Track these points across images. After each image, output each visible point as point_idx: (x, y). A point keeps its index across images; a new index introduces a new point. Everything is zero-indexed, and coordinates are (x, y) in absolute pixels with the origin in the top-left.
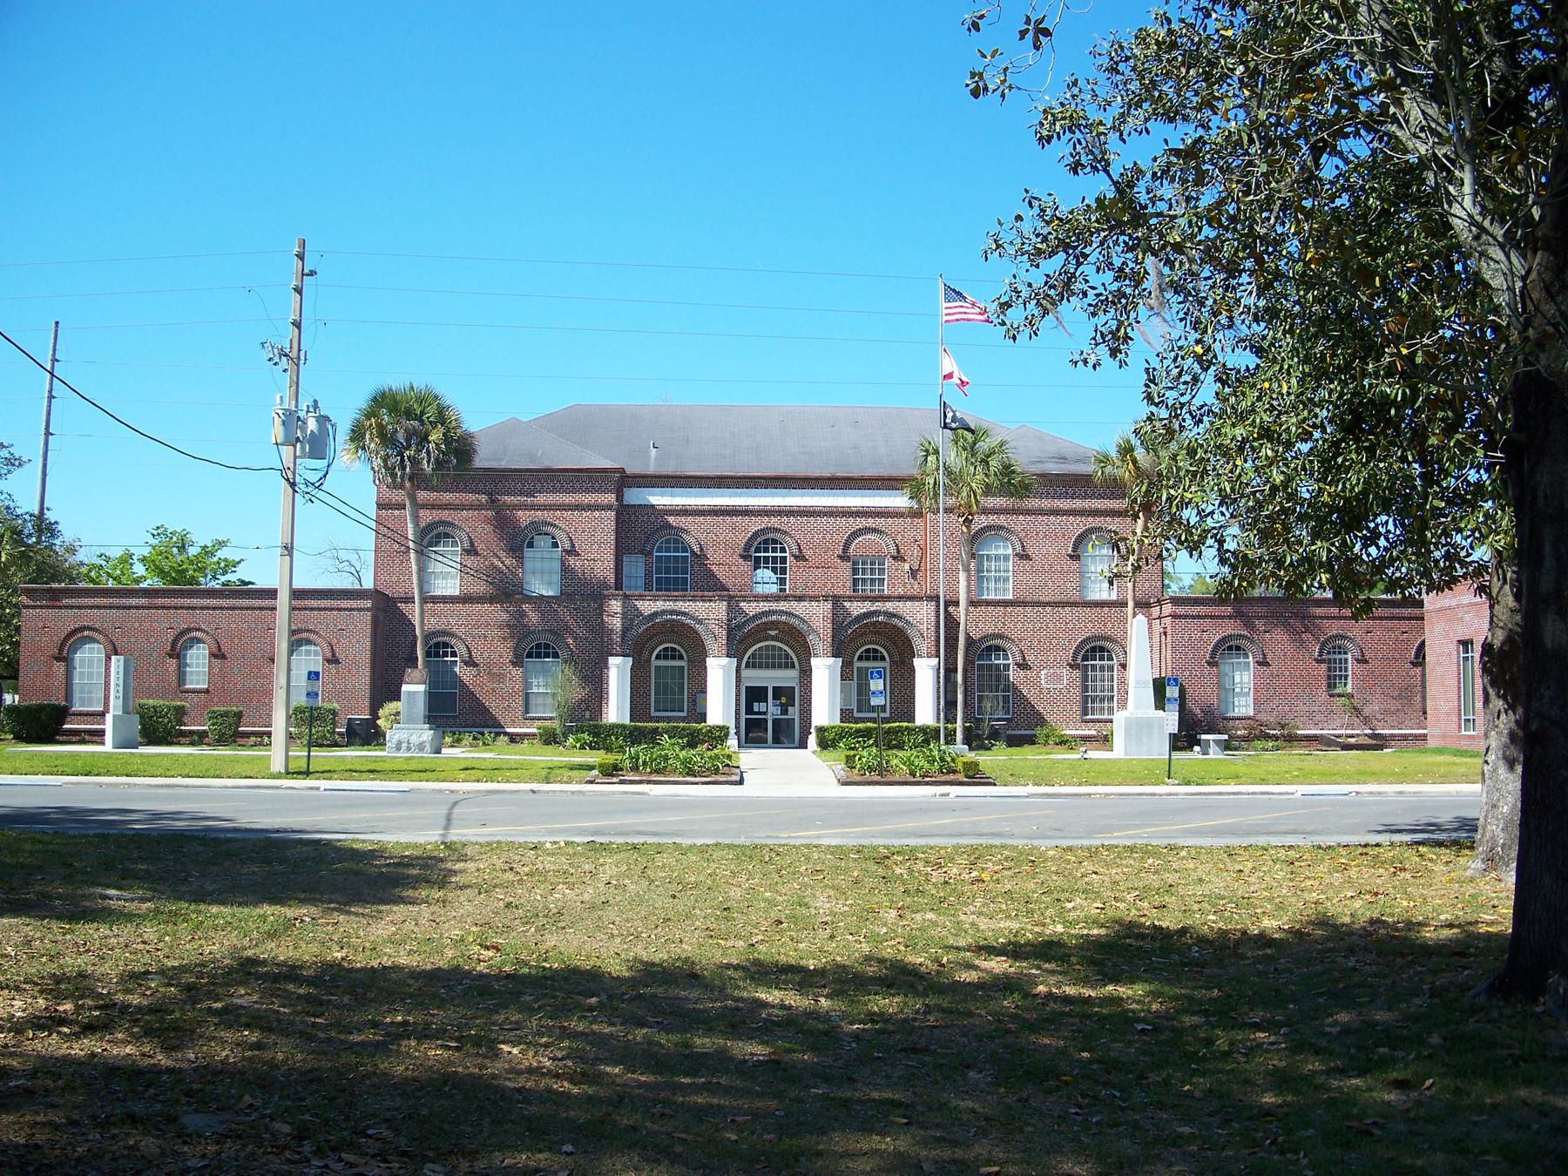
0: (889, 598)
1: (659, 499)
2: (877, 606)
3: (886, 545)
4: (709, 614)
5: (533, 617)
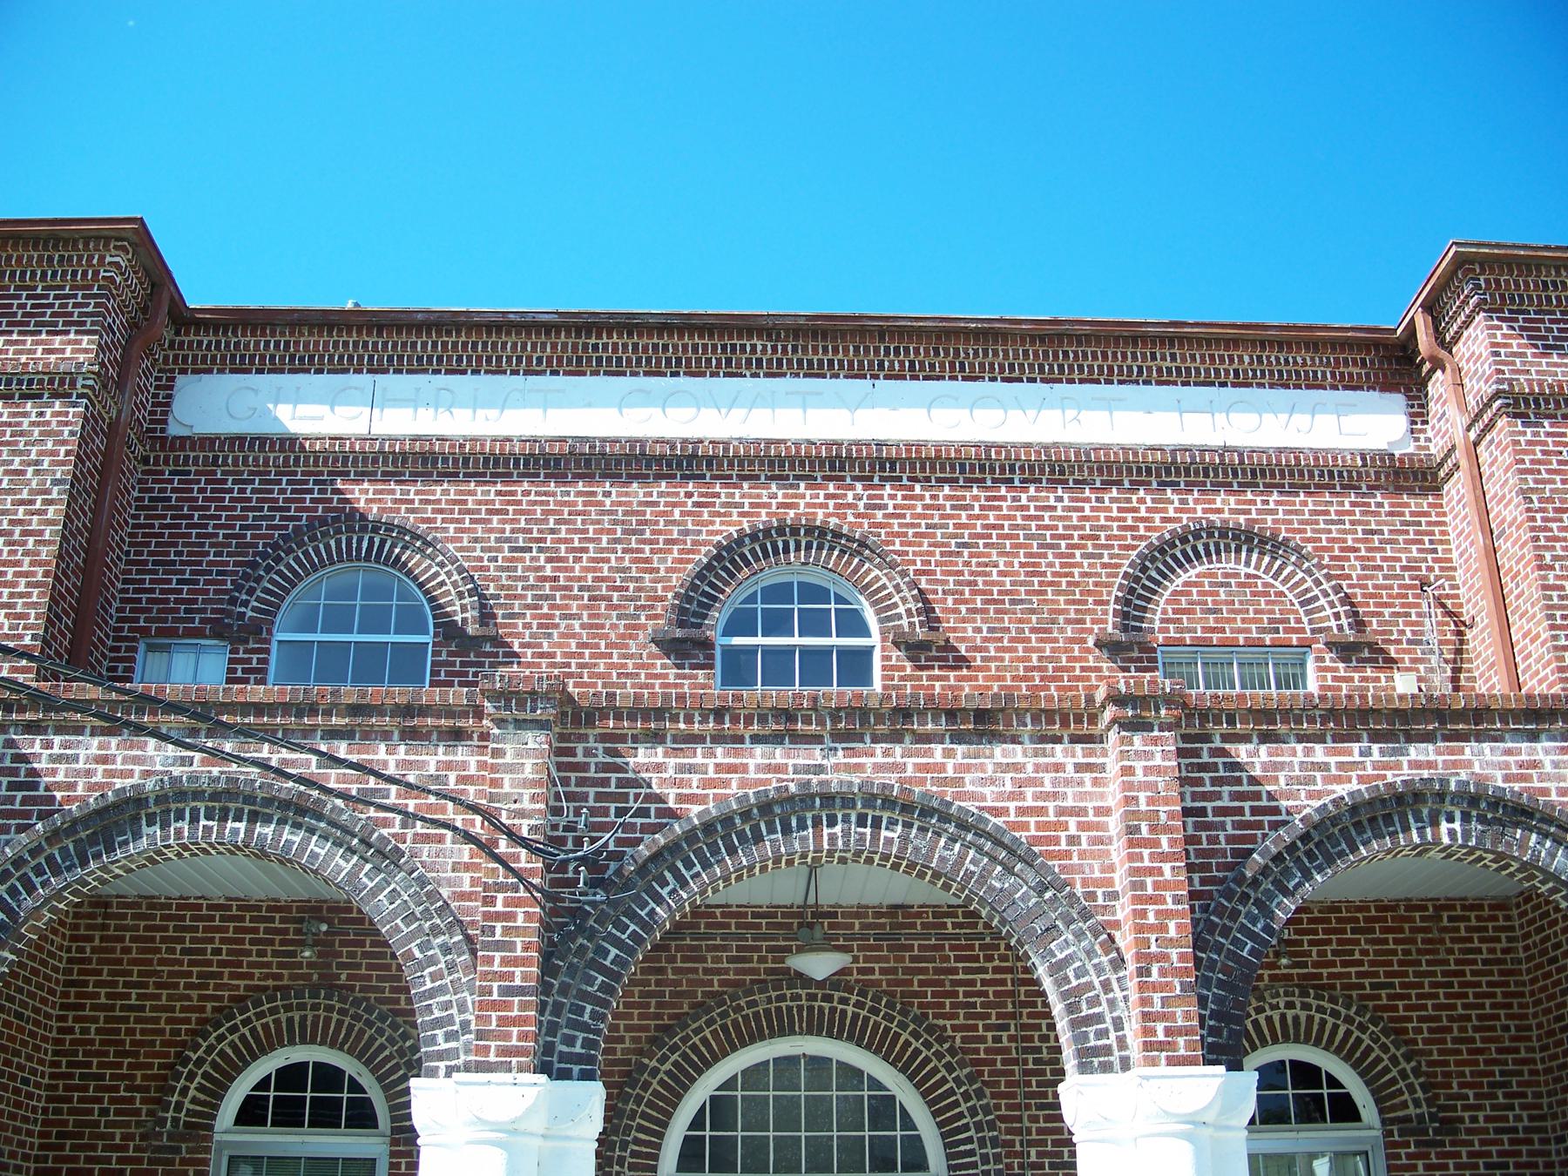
2: (1420, 761)
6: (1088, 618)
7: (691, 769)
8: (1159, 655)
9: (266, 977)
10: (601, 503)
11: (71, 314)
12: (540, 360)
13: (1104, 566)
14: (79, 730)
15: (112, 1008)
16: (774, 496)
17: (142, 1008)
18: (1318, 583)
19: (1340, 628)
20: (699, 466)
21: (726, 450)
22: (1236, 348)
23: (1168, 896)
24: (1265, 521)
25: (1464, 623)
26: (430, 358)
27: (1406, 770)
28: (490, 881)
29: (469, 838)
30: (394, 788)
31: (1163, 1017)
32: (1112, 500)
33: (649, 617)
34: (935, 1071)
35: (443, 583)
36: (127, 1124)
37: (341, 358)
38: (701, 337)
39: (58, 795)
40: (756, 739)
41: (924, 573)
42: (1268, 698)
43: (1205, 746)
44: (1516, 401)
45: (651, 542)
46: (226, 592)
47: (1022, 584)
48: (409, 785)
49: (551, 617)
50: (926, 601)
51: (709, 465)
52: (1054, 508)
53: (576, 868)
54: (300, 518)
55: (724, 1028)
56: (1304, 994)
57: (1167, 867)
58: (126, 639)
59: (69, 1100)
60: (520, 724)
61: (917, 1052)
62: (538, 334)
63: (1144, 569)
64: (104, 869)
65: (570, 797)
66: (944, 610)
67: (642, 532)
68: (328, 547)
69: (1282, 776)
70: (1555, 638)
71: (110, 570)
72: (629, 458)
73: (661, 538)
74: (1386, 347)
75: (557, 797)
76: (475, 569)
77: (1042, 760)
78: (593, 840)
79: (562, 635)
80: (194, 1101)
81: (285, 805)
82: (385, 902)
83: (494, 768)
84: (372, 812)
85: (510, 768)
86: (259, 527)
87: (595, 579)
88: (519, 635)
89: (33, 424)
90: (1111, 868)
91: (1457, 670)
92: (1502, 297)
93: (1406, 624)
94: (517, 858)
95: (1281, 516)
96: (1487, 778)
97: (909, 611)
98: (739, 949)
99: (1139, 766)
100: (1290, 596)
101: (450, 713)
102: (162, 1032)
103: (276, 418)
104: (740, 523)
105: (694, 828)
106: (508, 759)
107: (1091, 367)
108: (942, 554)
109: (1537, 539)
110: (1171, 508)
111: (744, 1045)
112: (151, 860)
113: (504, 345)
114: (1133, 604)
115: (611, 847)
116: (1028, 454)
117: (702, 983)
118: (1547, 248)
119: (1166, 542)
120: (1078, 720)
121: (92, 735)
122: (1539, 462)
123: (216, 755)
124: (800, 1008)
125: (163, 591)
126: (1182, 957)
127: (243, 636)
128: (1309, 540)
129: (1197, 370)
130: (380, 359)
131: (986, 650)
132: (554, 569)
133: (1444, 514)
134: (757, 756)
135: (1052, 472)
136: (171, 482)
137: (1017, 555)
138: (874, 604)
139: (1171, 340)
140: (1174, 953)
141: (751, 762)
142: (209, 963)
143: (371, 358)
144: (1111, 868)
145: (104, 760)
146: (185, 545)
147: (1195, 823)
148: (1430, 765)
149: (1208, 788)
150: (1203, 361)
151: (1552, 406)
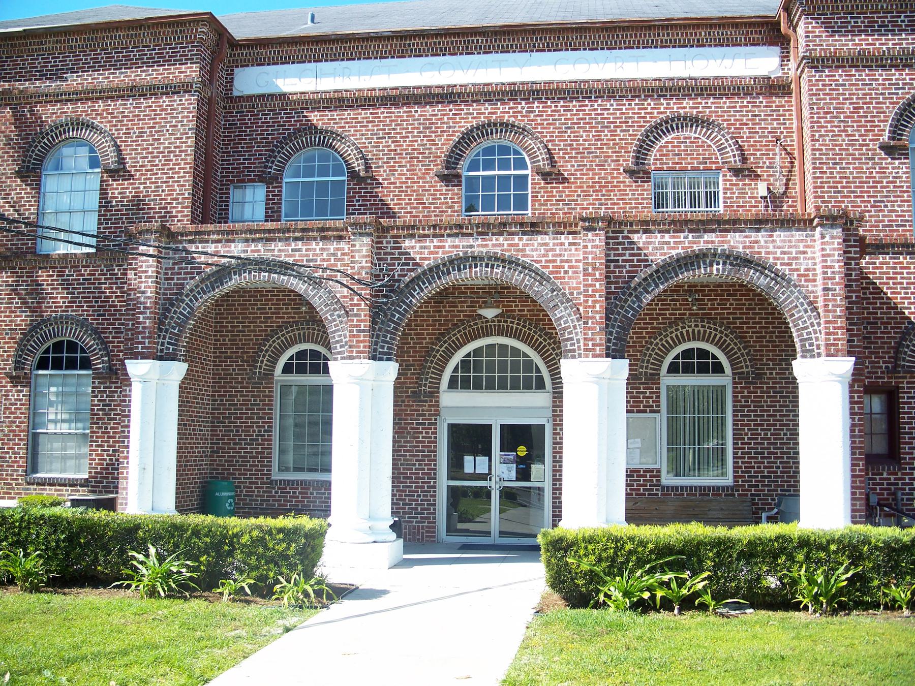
0: (731, 224)
1: (294, 80)
3: (719, 148)
4: (334, 265)
5: (58, 299)
7: (425, 247)
9: (289, 318)
10: (414, 116)
12: (386, 52)
13: (630, 135)
15: (233, 331)
16: (487, 109)
17: (244, 331)
18: (727, 140)
19: (735, 161)
21: (466, 89)
22: (698, 28)
23: (597, 295)
27: (702, 244)
31: (592, 340)
32: (636, 105)
34: (548, 350)
35: (350, 155)
36: (243, 374)
40: (449, 236)
41: (550, 141)
44: (813, 60)
45: (435, 132)
47: (593, 144)
50: (550, 154)
51: (459, 97)
52: (609, 109)
55: (465, 333)
56: (702, 321)
59: (221, 366)
60: (361, 234)
61: (541, 343)
66: (559, 158)
67: (431, 128)
68: (302, 141)
69: (650, 247)
70: (814, 173)
77: (556, 241)
79: (399, 174)
80: (266, 365)
82: (317, 298)
85: (358, 251)
87: (412, 150)
88: (381, 175)
89: (178, 105)
92: (814, 7)
95: (713, 109)
96: (735, 247)
98: (471, 302)
99: (590, 245)
100: (714, 147)
101: (337, 230)
102: (252, 340)
106: (357, 248)
107: (629, 41)
110: (662, 107)
111: (473, 340)
114: (641, 153)
117: (456, 316)
124: (495, 326)
125: (238, 164)
126: (601, 318)
128: (725, 120)
130: (318, 56)
132: (395, 146)
134: (449, 242)
135: (609, 92)
137: (591, 132)
138: (529, 156)
140: (598, 316)
141: (447, 245)
142: (268, 313)
148: (713, 242)
150: (682, 35)
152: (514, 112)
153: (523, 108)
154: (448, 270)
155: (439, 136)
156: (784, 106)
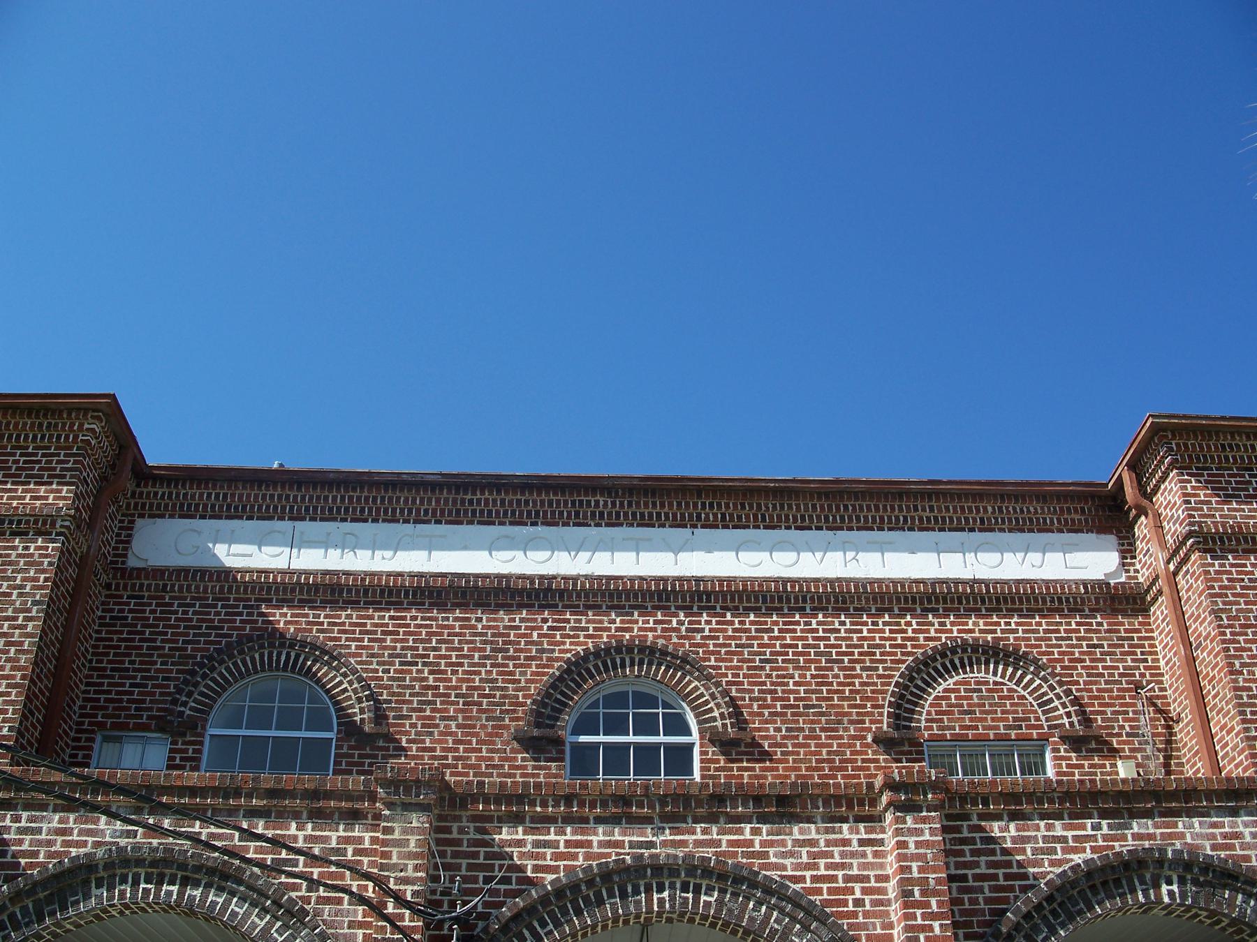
1: (247, 552)
2: (1141, 833)
6: (867, 719)
8: (925, 748)
10: (474, 627)
11: (54, 469)
12: (426, 511)
13: (879, 676)
14: (43, 807)
16: (614, 622)
18: (1052, 688)
20: (553, 597)
22: (982, 500)
24: (1008, 639)
25: (1172, 719)
26: (339, 509)
28: (379, 937)
29: (362, 900)
30: (302, 859)
32: (885, 624)
33: (511, 720)
37: (268, 507)
38: (555, 494)
39: (23, 861)
40: (599, 820)
41: (734, 683)
42: (1015, 783)
43: (965, 824)
44: (1205, 539)
45: (513, 658)
46: (169, 694)
47: (813, 692)
48: (314, 857)
49: (433, 718)
50: (736, 707)
51: (561, 597)
52: (838, 631)
53: (451, 927)
54: (231, 636)
57: (936, 925)
58: (86, 731)
60: (407, 807)
62: (425, 491)
63: (912, 679)
64: (58, 925)
65: (446, 867)
66: (750, 714)
68: (253, 660)
69: (1028, 847)
71: (76, 675)
72: (498, 591)
73: (522, 655)
74: (1100, 497)
75: (436, 867)
76: (372, 679)
78: (465, 903)
79: (441, 733)
81: (212, 871)
83: (385, 843)
84: (283, 879)
85: (398, 843)
86: (198, 642)
88: (407, 733)
89: (19, 556)
90: (891, 926)
91: (1168, 758)
92: (1190, 457)
93: (1125, 720)
94: (401, 917)
95: (1020, 634)
96: (1197, 847)
97: (722, 715)
99: (911, 840)
103: (215, 555)
104: (586, 643)
105: (548, 893)
106: (396, 835)
107: (866, 518)
108: (749, 668)
109: (1228, 649)
112: (97, 917)
113: (398, 499)
114: (904, 707)
115: (480, 909)
116: (817, 587)
118: (1223, 418)
119: (929, 657)
120: (861, 804)
121: (55, 811)
122: (1226, 588)
123: (155, 830)
125: (118, 693)
127: (182, 731)
128: (1044, 653)
129: (951, 519)
130: (299, 510)
131: (785, 746)
132: (435, 680)
133: (1152, 631)
134: (599, 836)
135: (837, 601)
136: (128, 604)
138: (693, 709)
139: (928, 495)
143: (292, 508)
144: (891, 926)
145: (63, 832)
146: (137, 655)
147: (958, 887)
148: (1151, 837)
149: (968, 858)
150: (955, 511)
151: (1234, 543)
152: (664, 630)
153: (681, 623)
154: (598, 895)
155: (521, 666)
156: (1138, 631)
